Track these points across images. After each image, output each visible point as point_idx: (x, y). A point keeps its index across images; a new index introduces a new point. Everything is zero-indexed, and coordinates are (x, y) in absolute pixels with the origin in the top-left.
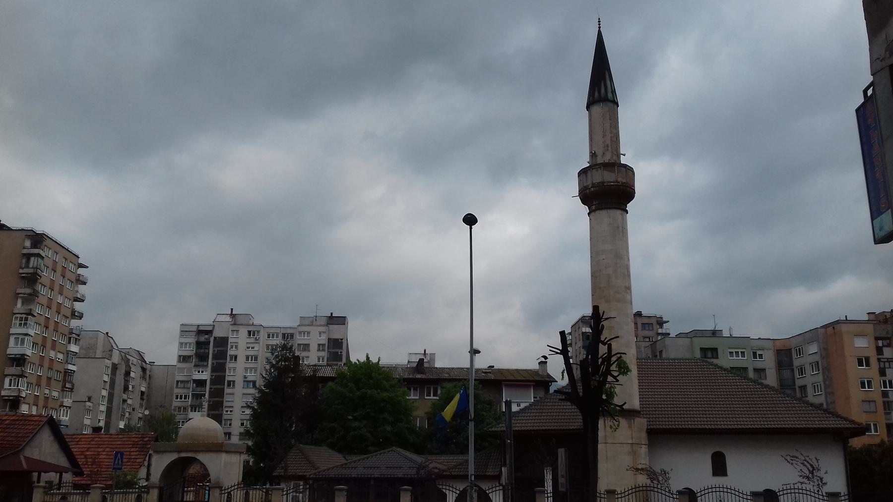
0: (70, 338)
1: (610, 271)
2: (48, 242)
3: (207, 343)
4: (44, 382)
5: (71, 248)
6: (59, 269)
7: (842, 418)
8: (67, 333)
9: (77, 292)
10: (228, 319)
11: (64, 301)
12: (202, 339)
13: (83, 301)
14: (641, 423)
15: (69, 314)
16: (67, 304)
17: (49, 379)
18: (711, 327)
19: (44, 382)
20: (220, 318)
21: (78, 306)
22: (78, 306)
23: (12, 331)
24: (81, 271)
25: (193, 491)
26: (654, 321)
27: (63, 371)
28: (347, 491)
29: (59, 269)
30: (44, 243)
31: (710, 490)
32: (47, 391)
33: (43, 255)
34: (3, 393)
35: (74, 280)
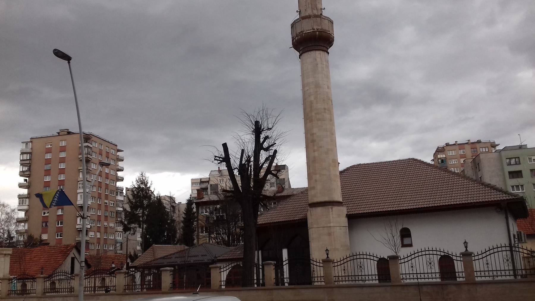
0: (117, 192)
1: (312, 98)
2: (94, 139)
3: (206, 189)
4: (103, 218)
5: (108, 139)
6: (104, 154)
7: (503, 192)
8: (115, 189)
9: (118, 165)
10: (217, 173)
11: (110, 172)
12: (204, 186)
13: (123, 170)
14: (344, 210)
15: (114, 178)
16: (112, 172)
17: (106, 217)
18: (518, 143)
19: (103, 218)
20: (213, 173)
21: (120, 174)
22: (120, 174)
23: (79, 191)
24: (119, 153)
25: (171, 271)
26: (489, 145)
27: (115, 211)
28: (275, 265)
29: (104, 154)
30: (92, 139)
31: (492, 251)
32: (106, 224)
33: (91, 146)
34: (77, 227)
35: (115, 159)
